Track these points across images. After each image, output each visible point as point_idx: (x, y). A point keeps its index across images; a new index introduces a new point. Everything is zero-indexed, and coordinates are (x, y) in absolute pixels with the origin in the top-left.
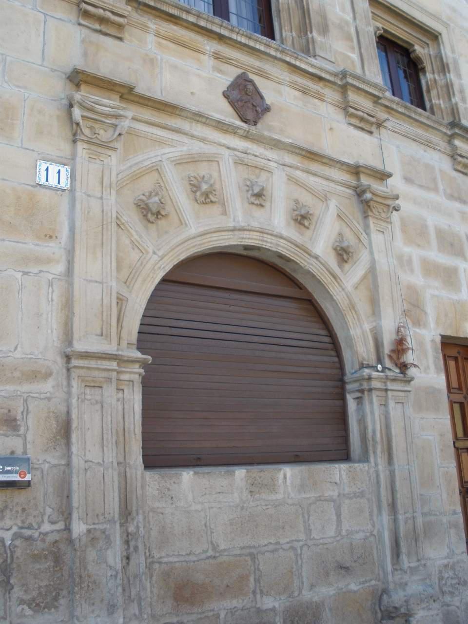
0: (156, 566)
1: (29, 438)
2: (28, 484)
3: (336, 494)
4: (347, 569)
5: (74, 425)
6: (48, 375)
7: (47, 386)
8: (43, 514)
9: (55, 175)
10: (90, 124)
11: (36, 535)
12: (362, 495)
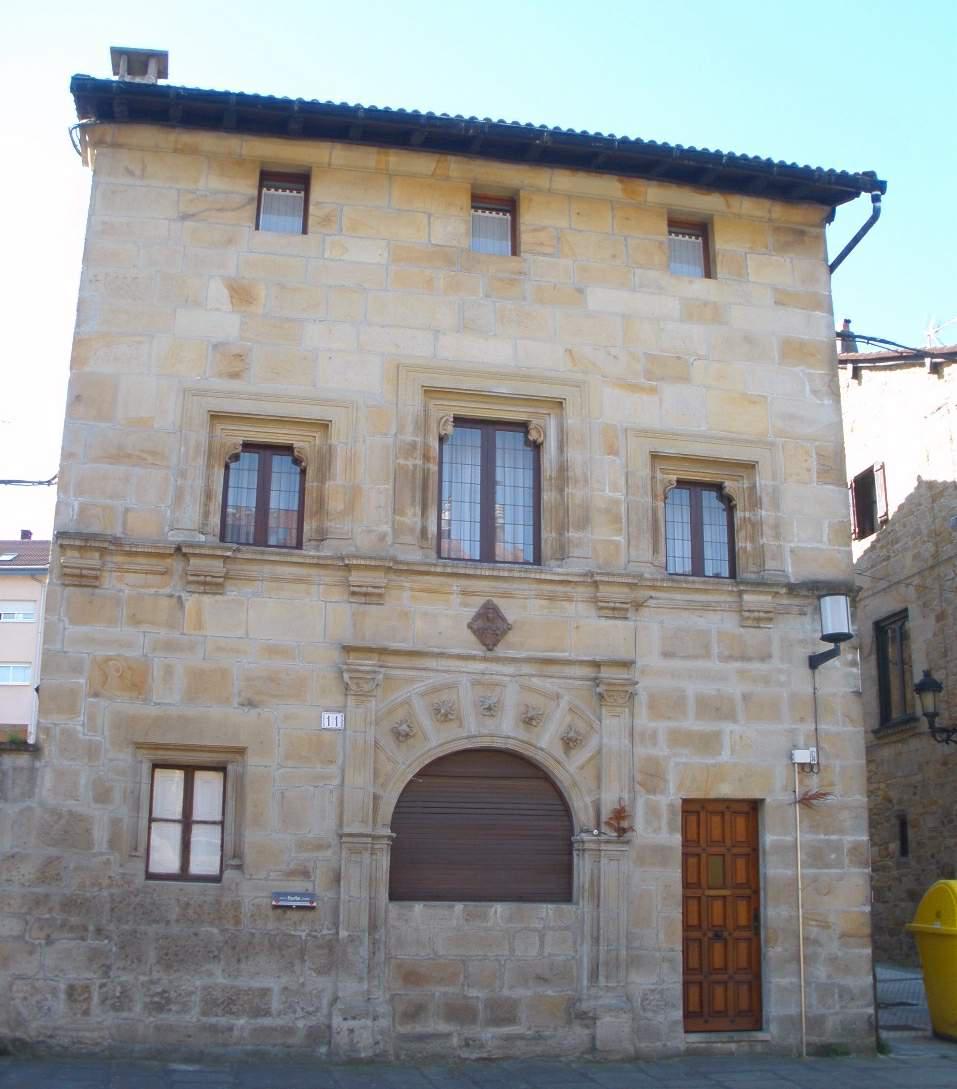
0: (393, 961)
1: (316, 883)
2: (314, 908)
3: (541, 926)
4: (546, 980)
5: (342, 875)
6: (329, 846)
7: (329, 853)
8: (323, 925)
9: (332, 720)
10: (355, 681)
11: (319, 935)
12: (567, 928)
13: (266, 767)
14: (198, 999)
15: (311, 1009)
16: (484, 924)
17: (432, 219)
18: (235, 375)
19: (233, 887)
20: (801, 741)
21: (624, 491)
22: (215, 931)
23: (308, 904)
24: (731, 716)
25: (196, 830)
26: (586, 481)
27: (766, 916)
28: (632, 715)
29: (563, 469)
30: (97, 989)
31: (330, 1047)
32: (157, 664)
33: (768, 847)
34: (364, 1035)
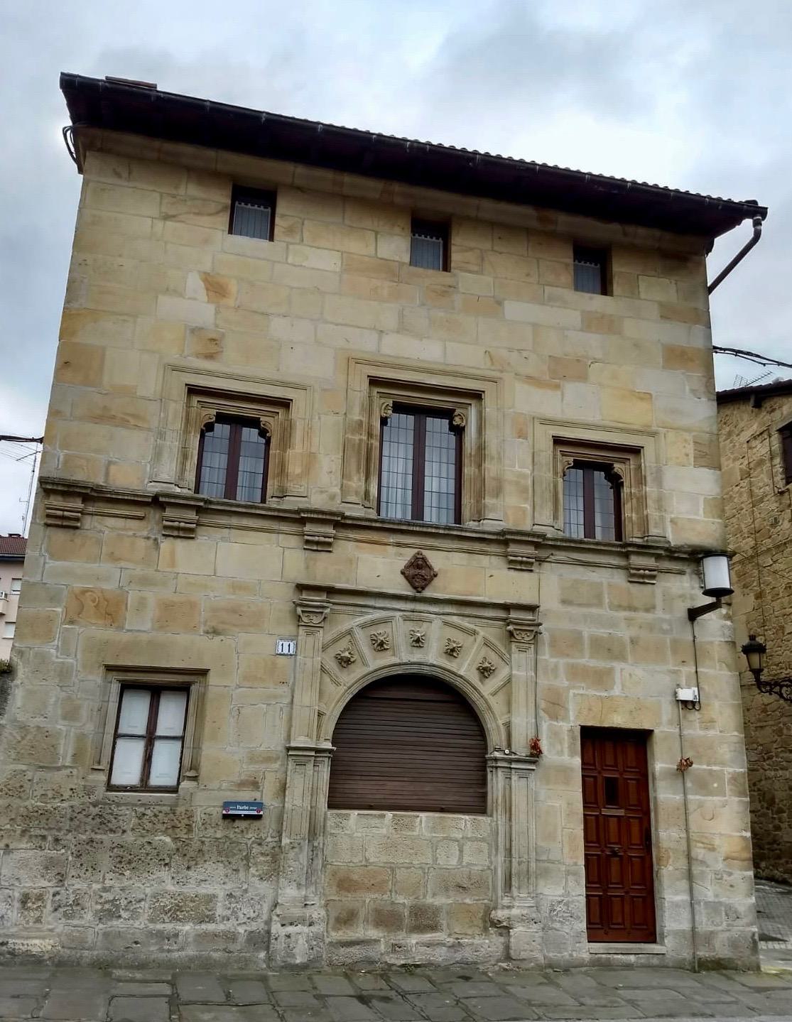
3: (461, 836)
6: (278, 758)
7: (276, 766)
10: (307, 614)
12: (483, 840)
13: (225, 686)
14: (147, 906)
15: (252, 915)
16: (410, 833)
17: (379, 236)
18: (210, 357)
19: (188, 798)
20: (683, 681)
21: (531, 468)
22: (168, 840)
23: (255, 813)
24: (621, 657)
25: (158, 745)
26: (500, 458)
27: (658, 837)
28: (536, 652)
29: (481, 448)
30: (51, 897)
31: (268, 952)
32: (132, 598)
33: (657, 774)
34: (298, 943)
